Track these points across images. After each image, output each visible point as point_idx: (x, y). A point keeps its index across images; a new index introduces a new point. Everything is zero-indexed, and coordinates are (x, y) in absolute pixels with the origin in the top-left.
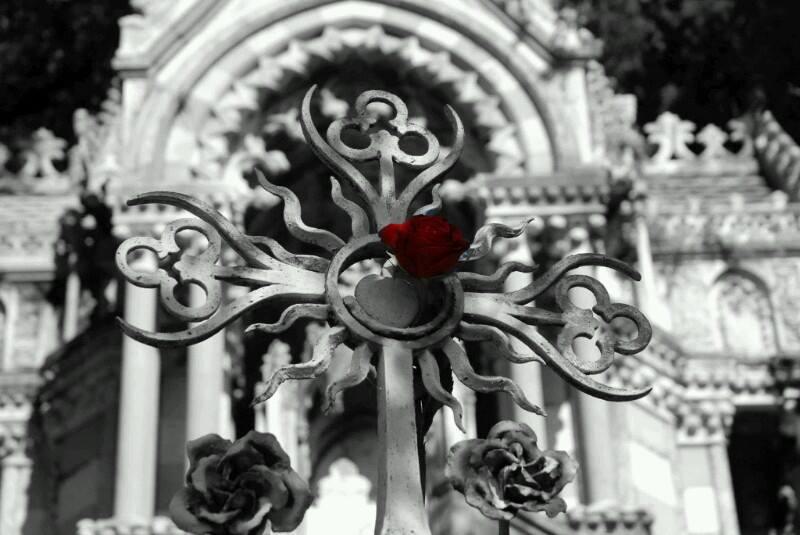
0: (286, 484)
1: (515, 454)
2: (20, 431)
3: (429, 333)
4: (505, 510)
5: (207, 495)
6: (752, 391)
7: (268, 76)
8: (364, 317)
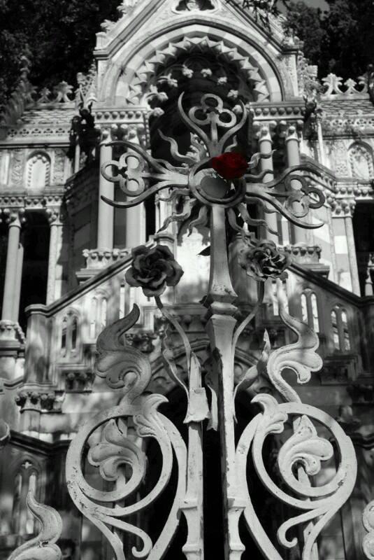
0: (172, 267)
1: (267, 253)
2: (57, 211)
3: (231, 201)
4: (262, 277)
5: (140, 271)
6: (364, 195)
7: (159, 58)
8: (204, 194)
